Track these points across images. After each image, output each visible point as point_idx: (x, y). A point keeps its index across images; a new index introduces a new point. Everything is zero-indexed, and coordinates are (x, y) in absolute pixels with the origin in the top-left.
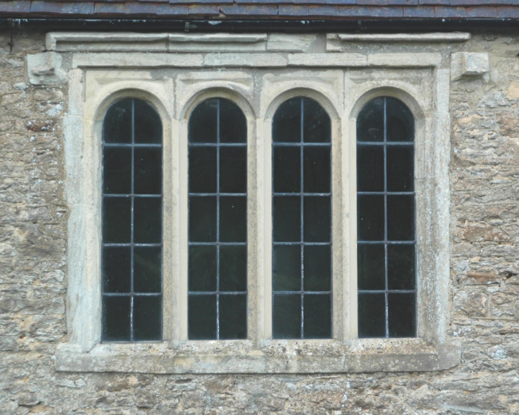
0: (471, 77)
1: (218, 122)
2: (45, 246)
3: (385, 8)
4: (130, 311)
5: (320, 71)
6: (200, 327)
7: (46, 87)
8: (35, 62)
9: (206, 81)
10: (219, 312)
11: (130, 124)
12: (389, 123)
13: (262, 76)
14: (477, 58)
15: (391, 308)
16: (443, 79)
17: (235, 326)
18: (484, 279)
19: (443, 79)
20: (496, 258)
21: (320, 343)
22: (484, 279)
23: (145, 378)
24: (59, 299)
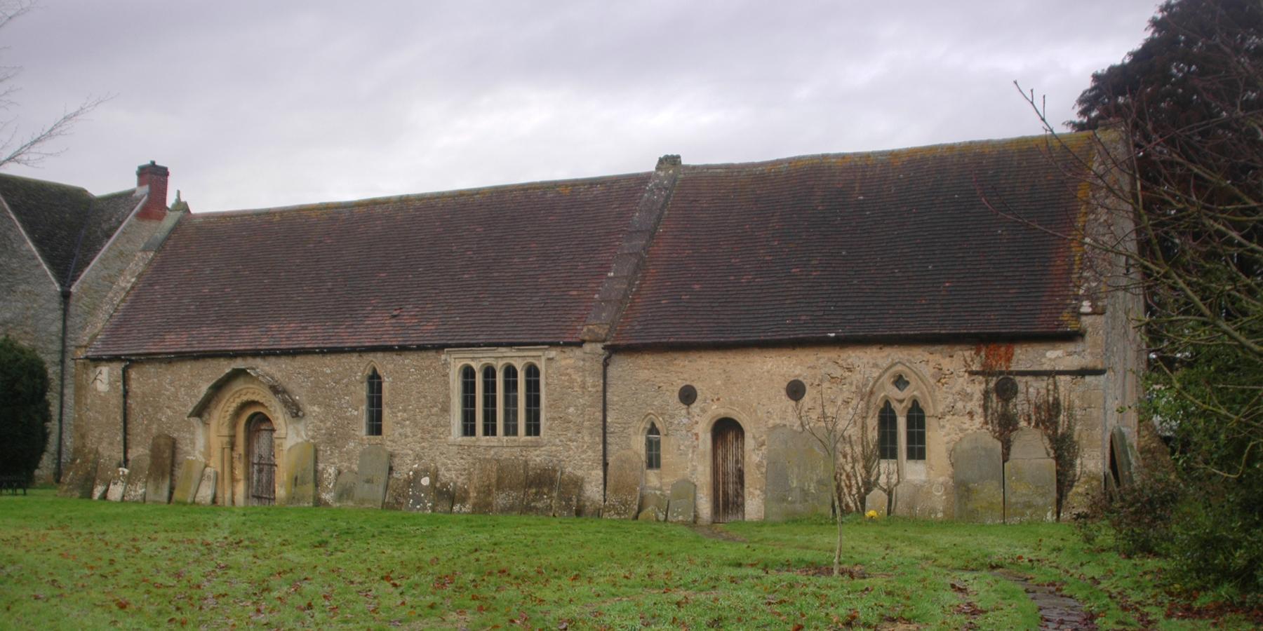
0: (549, 359)
1: (510, 372)
2: (446, 409)
3: (69, 323)
4: (469, 430)
5: (676, 355)
6: (486, 433)
7: (446, 364)
8: (443, 357)
9: (485, 361)
10: (490, 430)
11: (468, 373)
12: (532, 372)
13: (500, 359)
14: (552, 353)
15: (533, 429)
16: (543, 359)
17: (494, 434)
18: (554, 419)
19: (543, 359)
20: (1226, 337)
21: (513, 438)
22: (554, 419)
23: (469, 447)
24: (448, 425)
